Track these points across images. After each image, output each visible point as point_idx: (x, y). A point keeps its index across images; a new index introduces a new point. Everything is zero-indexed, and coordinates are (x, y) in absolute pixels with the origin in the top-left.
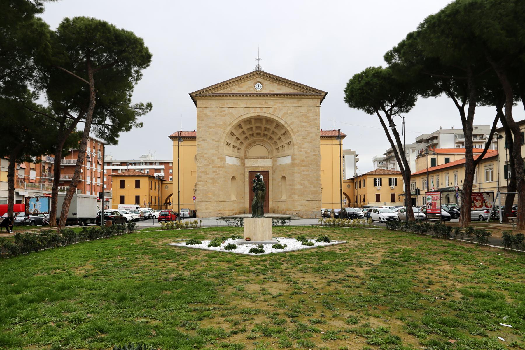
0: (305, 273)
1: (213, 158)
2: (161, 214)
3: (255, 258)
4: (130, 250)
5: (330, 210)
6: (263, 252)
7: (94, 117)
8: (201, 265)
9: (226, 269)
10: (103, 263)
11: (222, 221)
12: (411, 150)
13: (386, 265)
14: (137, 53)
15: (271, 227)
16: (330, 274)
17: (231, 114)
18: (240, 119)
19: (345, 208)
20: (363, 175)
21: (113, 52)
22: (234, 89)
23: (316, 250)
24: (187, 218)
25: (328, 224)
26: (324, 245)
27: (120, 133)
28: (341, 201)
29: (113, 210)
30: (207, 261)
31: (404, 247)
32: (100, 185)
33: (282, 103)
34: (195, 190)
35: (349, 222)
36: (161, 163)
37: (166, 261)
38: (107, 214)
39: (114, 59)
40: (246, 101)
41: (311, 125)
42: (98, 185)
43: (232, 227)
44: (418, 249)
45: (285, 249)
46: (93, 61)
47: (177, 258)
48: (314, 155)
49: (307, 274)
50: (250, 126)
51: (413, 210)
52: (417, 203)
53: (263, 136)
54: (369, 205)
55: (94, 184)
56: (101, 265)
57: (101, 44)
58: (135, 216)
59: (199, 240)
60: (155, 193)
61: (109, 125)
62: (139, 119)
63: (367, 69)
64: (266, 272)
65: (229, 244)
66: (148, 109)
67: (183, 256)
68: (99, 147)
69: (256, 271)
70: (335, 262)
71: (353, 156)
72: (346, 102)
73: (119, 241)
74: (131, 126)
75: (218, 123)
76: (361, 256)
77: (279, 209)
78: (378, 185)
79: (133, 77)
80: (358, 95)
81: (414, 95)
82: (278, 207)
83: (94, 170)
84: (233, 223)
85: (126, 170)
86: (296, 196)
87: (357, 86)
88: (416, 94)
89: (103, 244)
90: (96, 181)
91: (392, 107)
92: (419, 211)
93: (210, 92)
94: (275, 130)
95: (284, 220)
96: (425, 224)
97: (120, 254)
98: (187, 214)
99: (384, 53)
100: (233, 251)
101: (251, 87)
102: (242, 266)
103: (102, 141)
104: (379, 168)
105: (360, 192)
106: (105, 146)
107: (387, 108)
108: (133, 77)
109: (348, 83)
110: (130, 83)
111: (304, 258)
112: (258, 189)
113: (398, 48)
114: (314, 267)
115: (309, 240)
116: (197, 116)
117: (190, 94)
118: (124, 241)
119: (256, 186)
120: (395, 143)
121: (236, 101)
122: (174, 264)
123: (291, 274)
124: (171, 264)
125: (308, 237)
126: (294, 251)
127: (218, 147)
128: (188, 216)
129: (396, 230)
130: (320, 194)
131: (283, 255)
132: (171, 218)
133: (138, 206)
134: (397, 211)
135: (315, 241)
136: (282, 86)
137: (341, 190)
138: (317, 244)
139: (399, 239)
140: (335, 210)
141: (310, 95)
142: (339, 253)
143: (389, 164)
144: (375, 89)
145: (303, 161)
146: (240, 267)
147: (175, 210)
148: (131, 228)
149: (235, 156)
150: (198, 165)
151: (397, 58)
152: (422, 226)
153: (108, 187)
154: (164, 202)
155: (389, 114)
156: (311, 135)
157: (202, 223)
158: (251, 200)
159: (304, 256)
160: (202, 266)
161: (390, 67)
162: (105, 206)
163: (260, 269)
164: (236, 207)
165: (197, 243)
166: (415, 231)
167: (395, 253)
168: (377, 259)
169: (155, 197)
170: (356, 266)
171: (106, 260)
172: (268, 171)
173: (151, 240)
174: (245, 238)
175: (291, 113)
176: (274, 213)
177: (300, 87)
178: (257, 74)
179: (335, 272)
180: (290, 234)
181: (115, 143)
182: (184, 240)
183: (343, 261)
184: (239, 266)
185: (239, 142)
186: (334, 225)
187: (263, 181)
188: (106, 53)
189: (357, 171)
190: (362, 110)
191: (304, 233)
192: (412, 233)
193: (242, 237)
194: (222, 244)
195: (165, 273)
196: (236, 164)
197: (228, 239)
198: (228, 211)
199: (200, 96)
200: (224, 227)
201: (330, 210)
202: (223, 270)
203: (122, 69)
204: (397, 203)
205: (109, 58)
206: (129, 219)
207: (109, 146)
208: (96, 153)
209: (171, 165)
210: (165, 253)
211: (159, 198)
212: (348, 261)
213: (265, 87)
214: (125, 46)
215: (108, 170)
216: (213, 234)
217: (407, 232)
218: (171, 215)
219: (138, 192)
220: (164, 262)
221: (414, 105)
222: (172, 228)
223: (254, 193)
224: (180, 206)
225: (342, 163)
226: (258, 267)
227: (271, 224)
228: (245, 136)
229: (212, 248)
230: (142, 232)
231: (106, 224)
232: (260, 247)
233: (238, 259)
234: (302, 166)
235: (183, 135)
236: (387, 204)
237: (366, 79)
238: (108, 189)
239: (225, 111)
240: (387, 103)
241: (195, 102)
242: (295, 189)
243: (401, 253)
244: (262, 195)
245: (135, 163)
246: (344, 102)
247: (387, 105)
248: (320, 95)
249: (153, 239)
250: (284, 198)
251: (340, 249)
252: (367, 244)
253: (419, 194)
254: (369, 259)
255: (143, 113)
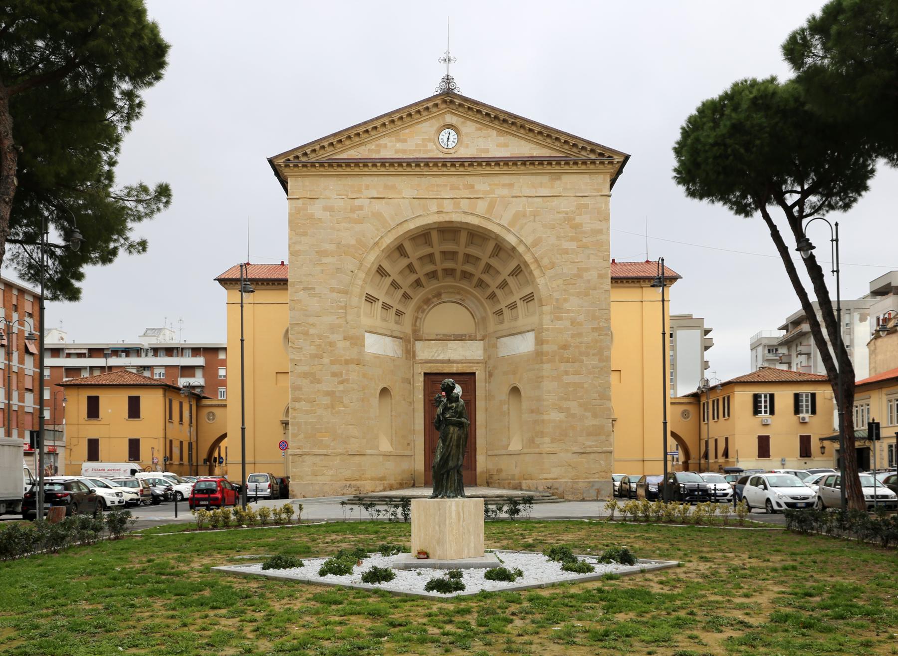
0: (568, 646)
1: (334, 337)
2: (197, 487)
3: (440, 605)
4: (114, 586)
5: (635, 478)
6: (462, 588)
7: (14, 222)
8: (301, 622)
9: (366, 633)
10: (42, 621)
11: (355, 507)
12: (856, 316)
13: (785, 626)
14: (128, 40)
15: (482, 523)
16: (634, 649)
17: (378, 215)
18: (401, 231)
19: (674, 474)
20: (723, 385)
21: (64, 35)
22: (385, 146)
23: (598, 584)
24: (265, 498)
25: (629, 514)
26: (618, 571)
27: (86, 269)
28: (666, 454)
29: (69, 478)
30: (317, 613)
31: (833, 580)
32: (31, 410)
33: (511, 185)
34: (286, 424)
35: (686, 510)
36: (196, 351)
37: (211, 613)
38: (51, 487)
39: (66, 57)
40: (416, 180)
41: (586, 247)
42: (27, 410)
43: (381, 522)
44: (874, 586)
45: (519, 583)
46: (6, 62)
47: (239, 605)
48: (594, 329)
49: (574, 647)
50: (427, 250)
51: (863, 481)
52: (872, 462)
53: (461, 279)
54: (740, 465)
55: (15, 408)
56: (37, 627)
57: (28, 13)
58: (129, 493)
59: (297, 557)
60: (182, 433)
61: (56, 246)
62: (136, 231)
63: (736, 85)
64: (468, 642)
65: (375, 568)
66: (160, 201)
67: (256, 599)
68: (28, 308)
69: (444, 639)
70: (648, 616)
71: (698, 333)
72: (679, 183)
73: (84, 561)
74: (116, 248)
75: (343, 242)
76: (717, 602)
77: (503, 475)
78: (766, 412)
79: (118, 111)
80: (710, 160)
81: (865, 160)
82: (499, 471)
83: (15, 369)
84: (385, 513)
85: (102, 368)
86: (547, 440)
87: (708, 136)
88: (870, 156)
89: (41, 568)
90: (21, 399)
91: (805, 194)
92: (878, 484)
93: (323, 155)
94: (494, 262)
95: (516, 503)
96: (893, 518)
97: (87, 595)
98: (265, 487)
99: (783, 37)
100: (384, 586)
101: (430, 140)
102: (408, 627)
103: (38, 290)
104: (766, 365)
105: (715, 429)
106: (46, 303)
107: (791, 199)
108: (118, 111)
109: (683, 128)
110: (111, 126)
111: (567, 605)
112: (448, 423)
113: (822, 19)
114: (592, 629)
115: (580, 558)
116: (291, 222)
117: (271, 161)
118: (98, 560)
119: (443, 413)
120: (813, 298)
121: (391, 181)
122: (230, 622)
123: (533, 648)
124: (224, 621)
125: (577, 550)
126: (540, 587)
127: (345, 307)
128: (268, 492)
129: (812, 535)
130: (608, 436)
131: (512, 598)
132: (223, 498)
133: (135, 466)
134: (816, 483)
135: (595, 561)
136: (510, 137)
137: (665, 424)
138: (601, 569)
139: (820, 558)
140: (649, 479)
141: (584, 163)
142: (659, 594)
143: (794, 354)
144: (758, 142)
145: (565, 347)
146: (402, 628)
147: (234, 476)
148: (118, 524)
149: (389, 333)
150: (293, 356)
151: (818, 50)
152: (887, 523)
153: (53, 415)
154: (204, 455)
155: (796, 214)
156: (586, 276)
157: (304, 511)
158: (429, 451)
159: (566, 601)
160: (304, 626)
161: (799, 77)
162: (45, 466)
163: (453, 634)
164: (393, 470)
165: (292, 565)
166: (867, 536)
167: (811, 595)
168: (760, 609)
169: (181, 443)
170: (704, 628)
171: (51, 611)
172: (475, 373)
173: (170, 558)
174: (414, 552)
175: (535, 215)
176: (488, 484)
177: (557, 139)
178: (445, 102)
179: (648, 642)
180: (530, 541)
181: (74, 295)
182: (258, 556)
183: (669, 614)
184: (400, 625)
185: (400, 293)
186: (647, 518)
187: (462, 401)
188: (43, 38)
189: (708, 374)
190: (721, 203)
191: (568, 538)
192: (858, 543)
193: (406, 550)
194: (355, 568)
195: (208, 645)
196: (390, 353)
197: (372, 555)
198: (372, 479)
199: (296, 166)
200: (362, 522)
201: (635, 478)
202: (358, 635)
203: (87, 86)
204: (817, 461)
205: (51, 54)
206: (113, 502)
207: (56, 303)
208: (21, 322)
209: (222, 356)
210: (207, 593)
211: (190, 444)
212: (682, 614)
213: (465, 140)
214: (96, 18)
215: (54, 370)
216: (333, 542)
217: (844, 540)
218: (222, 490)
219: (134, 429)
220: (206, 616)
221: (866, 188)
222: (226, 525)
223: (438, 434)
224: (247, 466)
225: (669, 353)
226: (449, 628)
227: (482, 515)
228: (413, 277)
229: (331, 578)
230: (147, 536)
231: (51, 514)
232: (453, 576)
233: (396, 607)
234: (562, 360)
235: (252, 274)
236: (787, 464)
237: (734, 115)
238: (55, 420)
239: (361, 208)
240: (790, 183)
241: (284, 184)
242: (543, 421)
243: (825, 596)
244: (459, 438)
245: (127, 352)
246: (674, 182)
247: (790, 188)
248: (611, 163)
249: (175, 555)
250: (515, 445)
251: (661, 583)
252: (734, 570)
253: (878, 438)
254: (740, 609)
255: (146, 214)
